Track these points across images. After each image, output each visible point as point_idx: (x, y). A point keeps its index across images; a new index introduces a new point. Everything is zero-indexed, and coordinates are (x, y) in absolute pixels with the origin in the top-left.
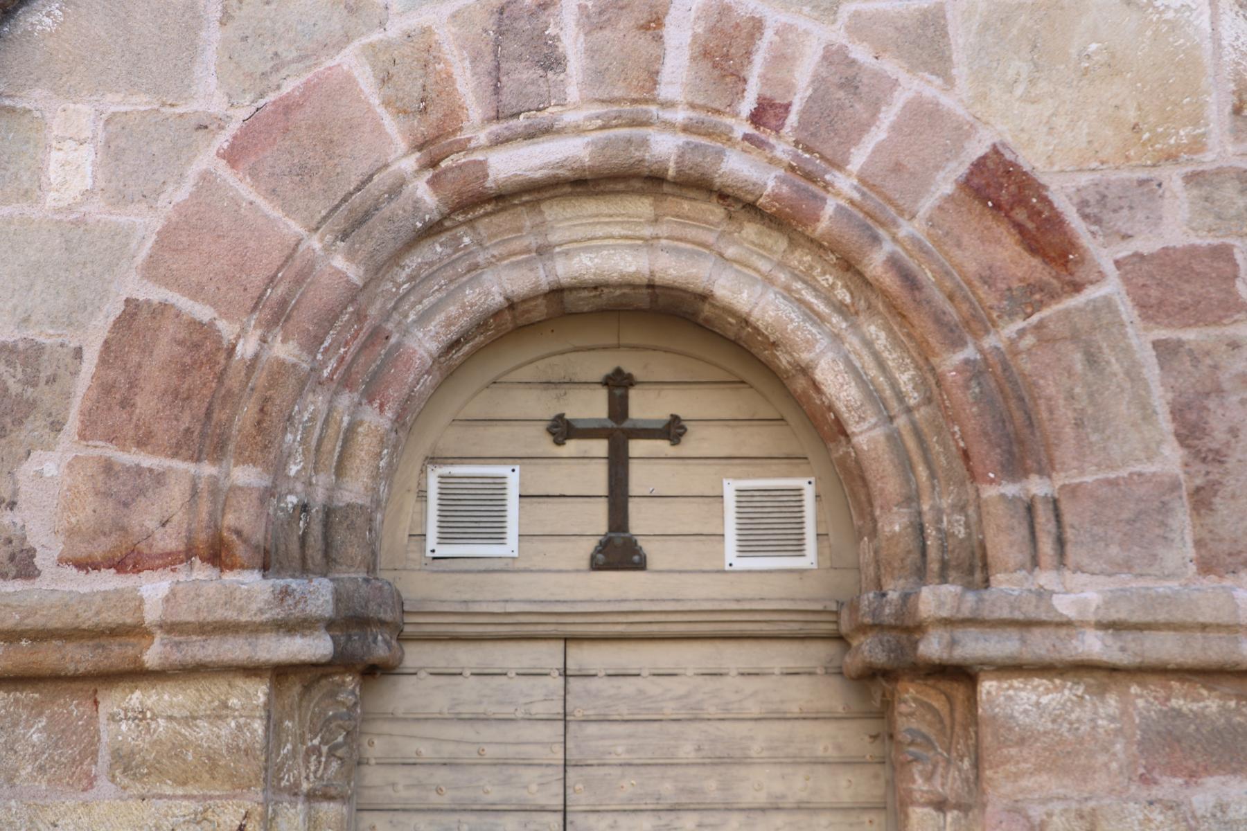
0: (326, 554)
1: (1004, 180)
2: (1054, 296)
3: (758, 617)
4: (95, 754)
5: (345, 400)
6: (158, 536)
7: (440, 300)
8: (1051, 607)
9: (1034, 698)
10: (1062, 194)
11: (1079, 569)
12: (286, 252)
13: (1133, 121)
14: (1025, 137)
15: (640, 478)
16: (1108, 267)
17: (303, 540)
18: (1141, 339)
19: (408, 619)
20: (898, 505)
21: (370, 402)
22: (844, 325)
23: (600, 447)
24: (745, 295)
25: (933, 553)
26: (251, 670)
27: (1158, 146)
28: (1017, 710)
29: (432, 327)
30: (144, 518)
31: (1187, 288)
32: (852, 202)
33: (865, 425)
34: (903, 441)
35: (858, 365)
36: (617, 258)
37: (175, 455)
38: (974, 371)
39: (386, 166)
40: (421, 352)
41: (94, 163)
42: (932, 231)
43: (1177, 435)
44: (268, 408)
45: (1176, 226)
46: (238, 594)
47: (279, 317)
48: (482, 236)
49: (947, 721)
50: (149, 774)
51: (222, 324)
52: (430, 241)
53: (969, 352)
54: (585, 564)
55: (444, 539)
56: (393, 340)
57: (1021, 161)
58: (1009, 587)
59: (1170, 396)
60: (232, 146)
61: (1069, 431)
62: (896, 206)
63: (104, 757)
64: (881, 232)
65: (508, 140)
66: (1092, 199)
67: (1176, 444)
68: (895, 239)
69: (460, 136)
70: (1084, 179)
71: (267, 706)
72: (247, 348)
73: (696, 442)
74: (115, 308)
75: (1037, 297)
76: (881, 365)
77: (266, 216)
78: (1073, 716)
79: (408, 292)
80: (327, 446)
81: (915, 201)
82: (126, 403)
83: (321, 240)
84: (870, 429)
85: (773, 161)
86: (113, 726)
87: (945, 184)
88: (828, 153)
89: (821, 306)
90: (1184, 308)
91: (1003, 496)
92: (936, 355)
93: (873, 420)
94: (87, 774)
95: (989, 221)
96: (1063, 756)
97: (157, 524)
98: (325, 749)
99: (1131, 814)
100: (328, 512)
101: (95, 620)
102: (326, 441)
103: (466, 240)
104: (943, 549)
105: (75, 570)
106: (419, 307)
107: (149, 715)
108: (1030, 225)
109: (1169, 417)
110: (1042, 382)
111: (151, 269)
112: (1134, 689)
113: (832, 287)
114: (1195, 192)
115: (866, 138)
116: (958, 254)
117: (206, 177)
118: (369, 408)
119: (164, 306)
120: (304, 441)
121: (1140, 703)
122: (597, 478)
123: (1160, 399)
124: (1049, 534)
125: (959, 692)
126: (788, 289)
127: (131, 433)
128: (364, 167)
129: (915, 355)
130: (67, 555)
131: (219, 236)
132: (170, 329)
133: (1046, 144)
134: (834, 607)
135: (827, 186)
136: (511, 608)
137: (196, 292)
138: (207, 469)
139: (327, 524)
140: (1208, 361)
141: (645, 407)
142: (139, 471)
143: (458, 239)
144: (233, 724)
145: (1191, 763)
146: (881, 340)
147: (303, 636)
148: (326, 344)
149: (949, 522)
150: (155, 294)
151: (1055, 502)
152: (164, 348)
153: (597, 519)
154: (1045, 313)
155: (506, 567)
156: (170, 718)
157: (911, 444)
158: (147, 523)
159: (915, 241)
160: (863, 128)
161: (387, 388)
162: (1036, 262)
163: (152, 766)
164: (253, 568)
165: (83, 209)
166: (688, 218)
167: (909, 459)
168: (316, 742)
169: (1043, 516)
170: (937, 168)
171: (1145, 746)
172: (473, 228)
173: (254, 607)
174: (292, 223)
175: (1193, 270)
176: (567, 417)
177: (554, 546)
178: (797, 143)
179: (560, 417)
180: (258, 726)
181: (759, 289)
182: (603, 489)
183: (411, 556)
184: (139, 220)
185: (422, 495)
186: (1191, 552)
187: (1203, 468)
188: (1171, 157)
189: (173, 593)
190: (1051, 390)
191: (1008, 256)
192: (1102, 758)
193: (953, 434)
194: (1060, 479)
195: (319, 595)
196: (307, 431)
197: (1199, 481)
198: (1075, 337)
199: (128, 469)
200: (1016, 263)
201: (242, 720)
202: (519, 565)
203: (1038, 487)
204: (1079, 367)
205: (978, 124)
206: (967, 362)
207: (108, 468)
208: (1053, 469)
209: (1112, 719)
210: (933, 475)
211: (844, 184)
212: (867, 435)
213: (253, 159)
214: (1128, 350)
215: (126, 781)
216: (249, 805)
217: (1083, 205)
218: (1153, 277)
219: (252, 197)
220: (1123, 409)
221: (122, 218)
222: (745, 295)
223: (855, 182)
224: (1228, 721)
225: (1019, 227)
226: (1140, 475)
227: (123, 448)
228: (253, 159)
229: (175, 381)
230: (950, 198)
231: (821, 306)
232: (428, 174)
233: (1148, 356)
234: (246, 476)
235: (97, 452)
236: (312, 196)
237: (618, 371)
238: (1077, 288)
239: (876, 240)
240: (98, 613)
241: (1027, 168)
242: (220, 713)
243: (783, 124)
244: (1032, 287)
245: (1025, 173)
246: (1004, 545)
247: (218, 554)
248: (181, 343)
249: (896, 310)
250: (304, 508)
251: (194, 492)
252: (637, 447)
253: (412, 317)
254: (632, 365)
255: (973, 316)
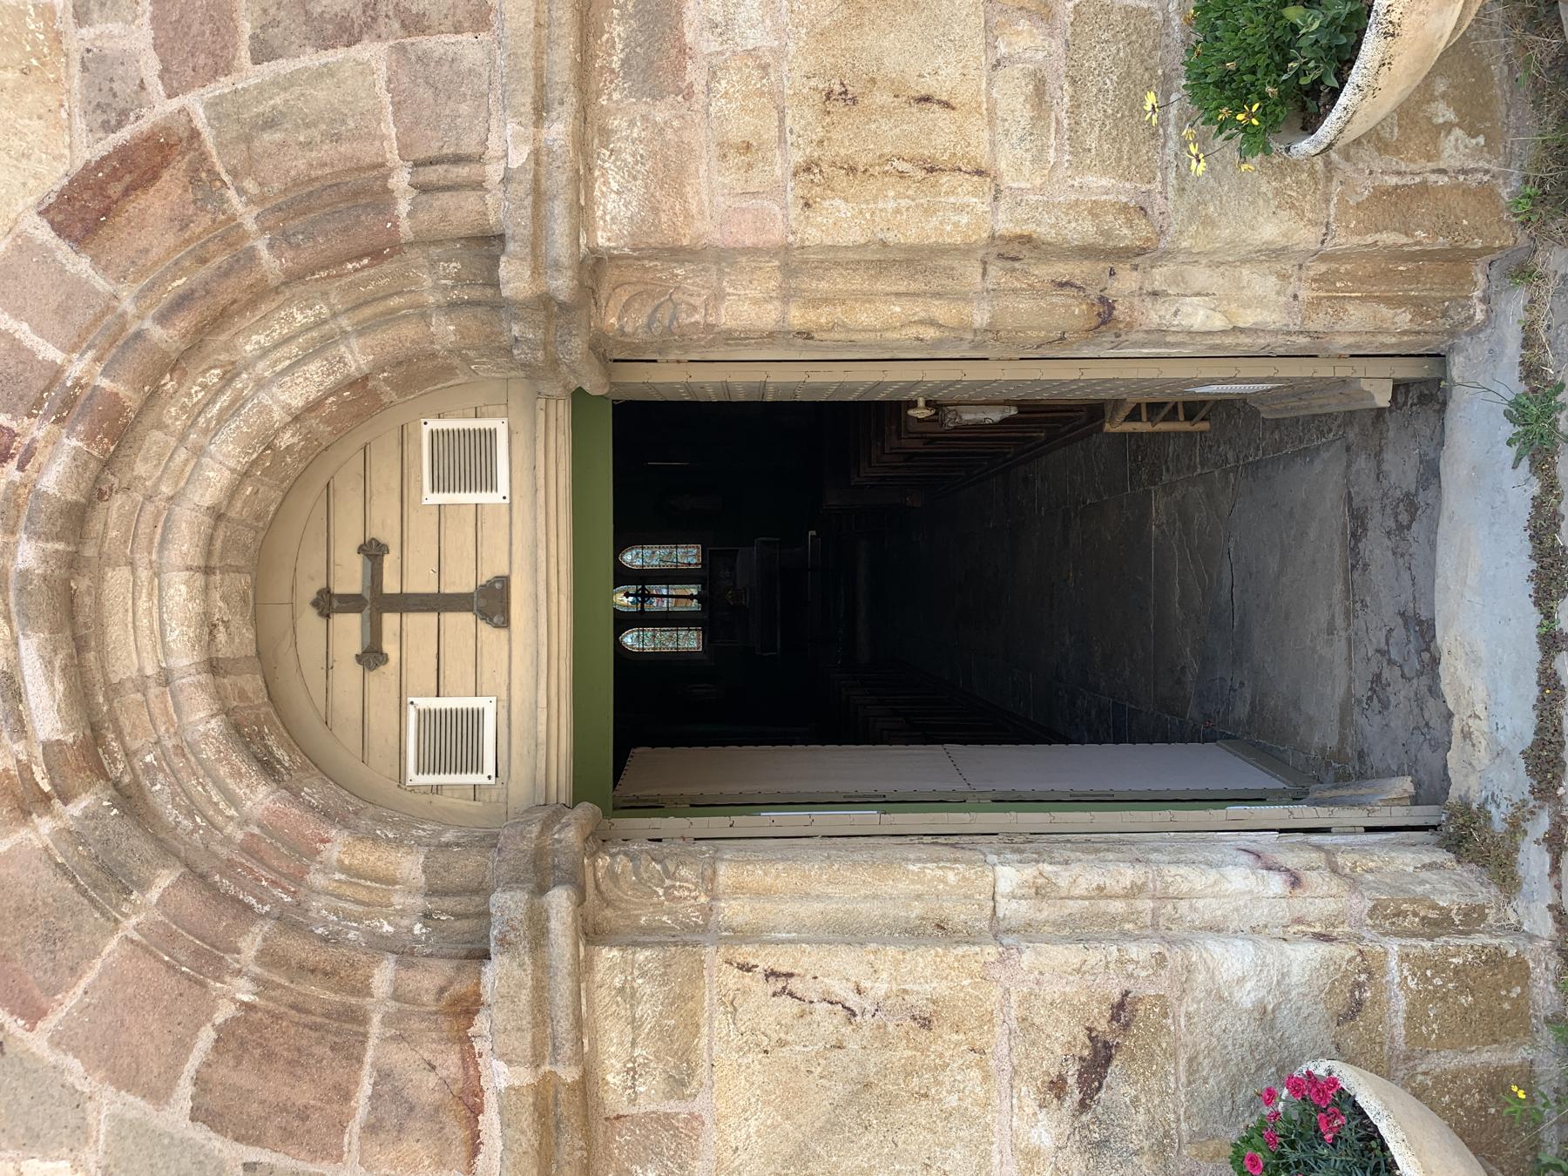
0: (476, 892)
1: (78, 205)
2: (204, 157)
3: (552, 473)
4: (667, 1116)
5: (317, 879)
6: (445, 1073)
7: (214, 783)
8: (522, 169)
9: (613, 196)
10: (90, 148)
11: (484, 143)
12: (139, 952)
13: (18, 74)
14: (31, 183)
15: (421, 582)
16: (175, 104)
17: (459, 916)
18: (249, 75)
19: (553, 799)
20: (428, 325)
21: (319, 852)
22: (245, 376)
23: (390, 621)
24: (211, 474)
25: (476, 293)
26: (582, 970)
27: (46, 50)
28: (624, 213)
29: (241, 792)
30: (426, 1088)
31: (195, 29)
32: (97, 359)
33: (348, 357)
34: (365, 320)
35: (287, 363)
36: (170, 604)
37: (360, 1061)
38: (282, 240)
39: (46, 849)
40: (267, 802)
41: (43, 1160)
42: (131, 277)
43: (349, 45)
44: (310, 965)
45: (132, 37)
46: (504, 991)
47: (214, 958)
48: (141, 738)
49: (640, 288)
50: (688, 1062)
51: (219, 1018)
52: (150, 796)
53: (261, 245)
54: (503, 633)
55: (478, 767)
56: (257, 831)
57: (57, 188)
58: (499, 207)
59: (309, 50)
60: (22, 1016)
61: (344, 148)
62: (103, 314)
63: (671, 1106)
64: (132, 330)
65: (20, 720)
66: (101, 118)
67: (358, 46)
68: (140, 317)
69: (14, 772)
70: (80, 124)
71: (623, 946)
72: (245, 993)
73: (385, 529)
74: (200, 1134)
75: (204, 175)
76: (286, 340)
77: (100, 976)
78: (630, 159)
79: (204, 817)
80: (363, 895)
81: (97, 293)
82: (303, 1116)
83: (126, 916)
84: (352, 352)
85: (54, 442)
86: (641, 1101)
87: (80, 265)
88: (41, 384)
89: (225, 399)
90: (216, 32)
91: (409, 215)
92: (264, 279)
93: (343, 349)
94: (687, 1122)
95: (120, 220)
96: (669, 171)
97: (432, 1074)
98: (668, 882)
99: (721, 110)
100: (432, 892)
101: (529, 1134)
102: (359, 897)
103: (149, 758)
104: (472, 284)
105: (480, 1157)
106: (222, 805)
107: (630, 1065)
108: (128, 178)
109: (331, 51)
110: (293, 173)
111: (159, 1095)
112: (603, 101)
113: (204, 387)
114: (95, 16)
115: (27, 344)
116: (154, 254)
117: (56, 1042)
118: (325, 854)
119: (198, 1081)
120: (359, 920)
121: (616, 96)
122: (421, 624)
123: (311, 59)
124: (441, 171)
125: (611, 275)
126: (206, 431)
127: (336, 1107)
128: (47, 874)
129: (274, 305)
130: (464, 1167)
131: (122, 1025)
132: (222, 1072)
133: (40, 162)
134: (541, 403)
135: (77, 383)
136: (543, 702)
137: (183, 1046)
138: (375, 1027)
139: (444, 893)
140: (272, 11)
141: (350, 580)
142: (375, 1097)
143: (148, 768)
144: (640, 981)
145: (674, 52)
146: (260, 338)
147: (548, 919)
148: (254, 902)
149: (445, 277)
150: (185, 1089)
151: (416, 164)
152: (244, 1078)
153: (460, 623)
154: (220, 168)
155: (506, 709)
156: (634, 1044)
157: (367, 312)
158: (431, 1085)
159: (138, 298)
160: (16, 346)
161: (304, 836)
162: (166, 175)
163: (680, 1058)
164: (480, 972)
165: (93, 1170)
166: (128, 530)
167: (383, 314)
168: (661, 892)
169: (433, 174)
170: (63, 271)
171: (657, 95)
172: (135, 753)
173: (517, 973)
174: (107, 950)
175: (178, 21)
176: (359, 651)
177: (486, 665)
178: (30, 415)
179: (359, 658)
180: (642, 955)
181: (205, 460)
182: (432, 618)
183: (494, 798)
184: (105, 1111)
185: (437, 789)
186: (467, 37)
187: (381, 20)
188: (58, 38)
189: (501, 1056)
190: (301, 164)
191: (160, 200)
192: (669, 134)
193: (356, 270)
194: (393, 157)
195: (508, 904)
196: (348, 916)
197: (396, 25)
198: (248, 139)
199: (374, 1109)
200: (168, 194)
201: (636, 973)
202: (504, 696)
203: (401, 180)
204: (278, 136)
205: (17, 230)
206: (271, 247)
207: (372, 1128)
208: (383, 165)
209: (632, 124)
210: (400, 293)
211: (78, 368)
212: (356, 357)
213: (36, 992)
214: (260, 88)
215: (694, 1083)
216: (719, 960)
217: (108, 128)
218: (186, 60)
219: (80, 991)
220: (321, 95)
221: (101, 1128)
222: (211, 474)
223: (75, 356)
224: (631, 16)
225: (126, 192)
226: (389, 81)
227: (351, 1115)
228: (36, 992)
229: (281, 1065)
230: (95, 259)
231: (225, 399)
232: (57, 803)
233: (268, 69)
234: (383, 976)
235: (355, 1139)
236: (78, 928)
237: (315, 604)
238: (195, 134)
239: (138, 335)
240: (523, 1132)
241: (65, 181)
242: (627, 994)
243: (8, 429)
244: (194, 180)
245: (71, 183)
246: (462, 211)
247: (466, 1008)
248: (239, 1063)
249: (220, 319)
250: (427, 916)
251: (401, 1038)
252: (390, 585)
253: (232, 812)
254: (310, 591)
255: (223, 238)
